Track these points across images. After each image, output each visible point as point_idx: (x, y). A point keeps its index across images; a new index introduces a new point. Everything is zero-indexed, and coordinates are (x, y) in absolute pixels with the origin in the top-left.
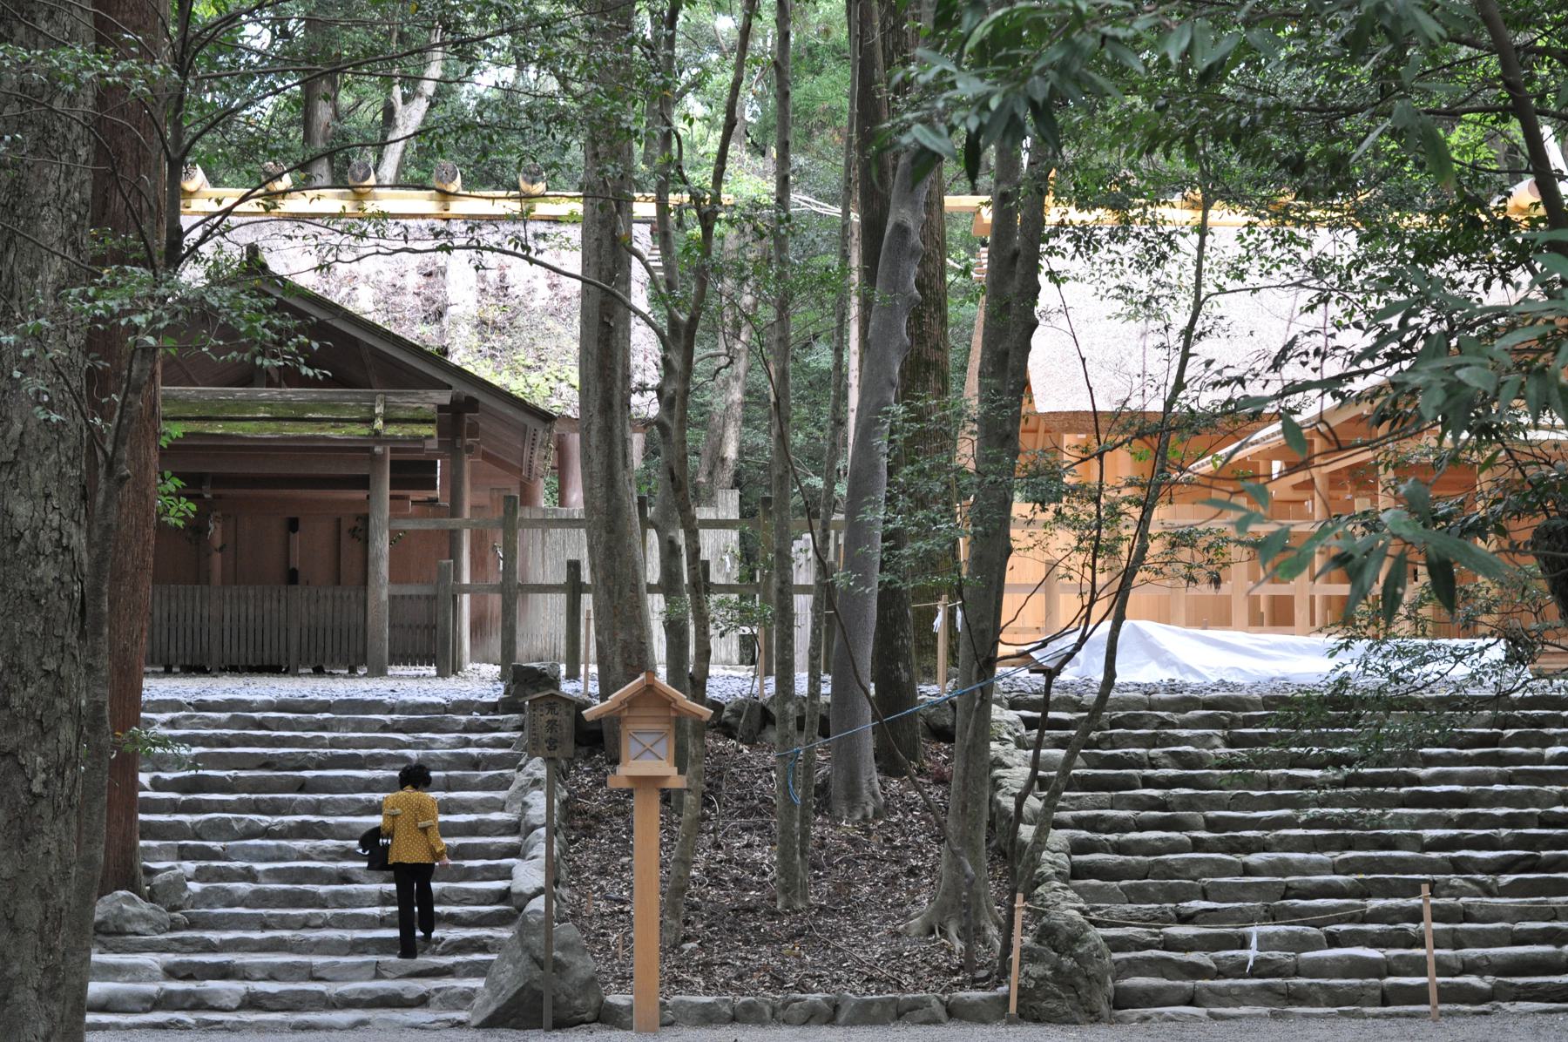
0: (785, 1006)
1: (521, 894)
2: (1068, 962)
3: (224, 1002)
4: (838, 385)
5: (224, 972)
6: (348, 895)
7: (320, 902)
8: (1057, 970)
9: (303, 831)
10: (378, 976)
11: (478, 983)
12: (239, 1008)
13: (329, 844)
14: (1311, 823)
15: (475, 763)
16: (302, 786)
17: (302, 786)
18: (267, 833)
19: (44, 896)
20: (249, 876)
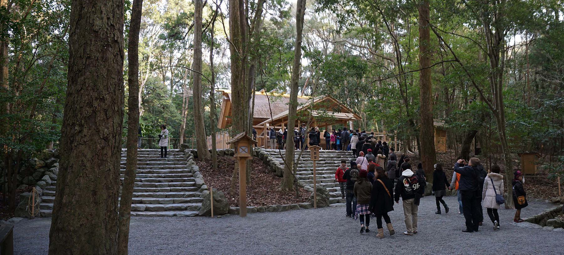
0: (268, 208)
1: (199, 185)
2: (324, 196)
3: (142, 209)
4: (237, 67)
5: (141, 202)
6: (162, 185)
7: (156, 186)
8: (322, 197)
9: (149, 172)
10: (174, 203)
11: (200, 204)
12: (145, 211)
13: (155, 175)
14: (326, 170)
15: (178, 160)
16: (147, 164)
17: (147, 164)
18: (142, 173)
19: (108, 188)
20: (141, 181)
